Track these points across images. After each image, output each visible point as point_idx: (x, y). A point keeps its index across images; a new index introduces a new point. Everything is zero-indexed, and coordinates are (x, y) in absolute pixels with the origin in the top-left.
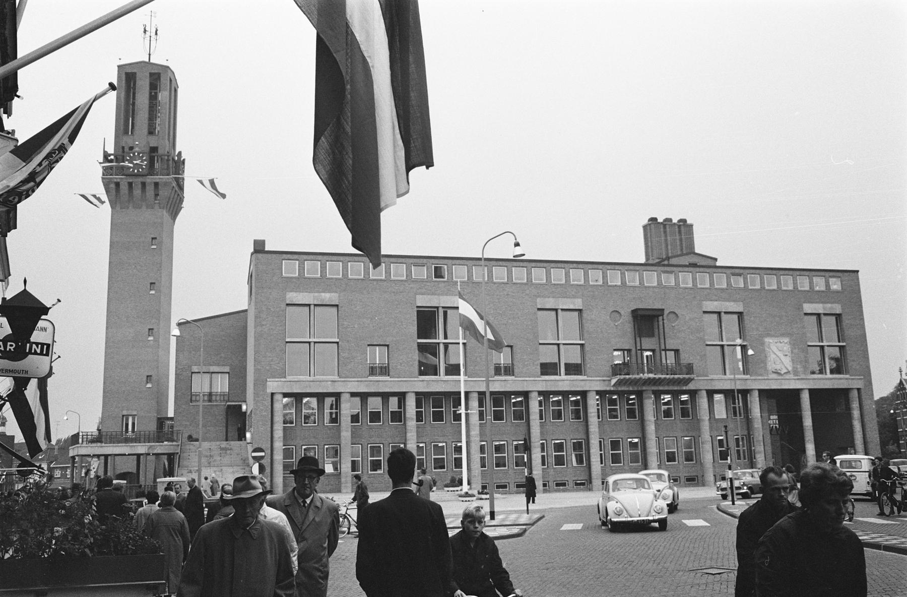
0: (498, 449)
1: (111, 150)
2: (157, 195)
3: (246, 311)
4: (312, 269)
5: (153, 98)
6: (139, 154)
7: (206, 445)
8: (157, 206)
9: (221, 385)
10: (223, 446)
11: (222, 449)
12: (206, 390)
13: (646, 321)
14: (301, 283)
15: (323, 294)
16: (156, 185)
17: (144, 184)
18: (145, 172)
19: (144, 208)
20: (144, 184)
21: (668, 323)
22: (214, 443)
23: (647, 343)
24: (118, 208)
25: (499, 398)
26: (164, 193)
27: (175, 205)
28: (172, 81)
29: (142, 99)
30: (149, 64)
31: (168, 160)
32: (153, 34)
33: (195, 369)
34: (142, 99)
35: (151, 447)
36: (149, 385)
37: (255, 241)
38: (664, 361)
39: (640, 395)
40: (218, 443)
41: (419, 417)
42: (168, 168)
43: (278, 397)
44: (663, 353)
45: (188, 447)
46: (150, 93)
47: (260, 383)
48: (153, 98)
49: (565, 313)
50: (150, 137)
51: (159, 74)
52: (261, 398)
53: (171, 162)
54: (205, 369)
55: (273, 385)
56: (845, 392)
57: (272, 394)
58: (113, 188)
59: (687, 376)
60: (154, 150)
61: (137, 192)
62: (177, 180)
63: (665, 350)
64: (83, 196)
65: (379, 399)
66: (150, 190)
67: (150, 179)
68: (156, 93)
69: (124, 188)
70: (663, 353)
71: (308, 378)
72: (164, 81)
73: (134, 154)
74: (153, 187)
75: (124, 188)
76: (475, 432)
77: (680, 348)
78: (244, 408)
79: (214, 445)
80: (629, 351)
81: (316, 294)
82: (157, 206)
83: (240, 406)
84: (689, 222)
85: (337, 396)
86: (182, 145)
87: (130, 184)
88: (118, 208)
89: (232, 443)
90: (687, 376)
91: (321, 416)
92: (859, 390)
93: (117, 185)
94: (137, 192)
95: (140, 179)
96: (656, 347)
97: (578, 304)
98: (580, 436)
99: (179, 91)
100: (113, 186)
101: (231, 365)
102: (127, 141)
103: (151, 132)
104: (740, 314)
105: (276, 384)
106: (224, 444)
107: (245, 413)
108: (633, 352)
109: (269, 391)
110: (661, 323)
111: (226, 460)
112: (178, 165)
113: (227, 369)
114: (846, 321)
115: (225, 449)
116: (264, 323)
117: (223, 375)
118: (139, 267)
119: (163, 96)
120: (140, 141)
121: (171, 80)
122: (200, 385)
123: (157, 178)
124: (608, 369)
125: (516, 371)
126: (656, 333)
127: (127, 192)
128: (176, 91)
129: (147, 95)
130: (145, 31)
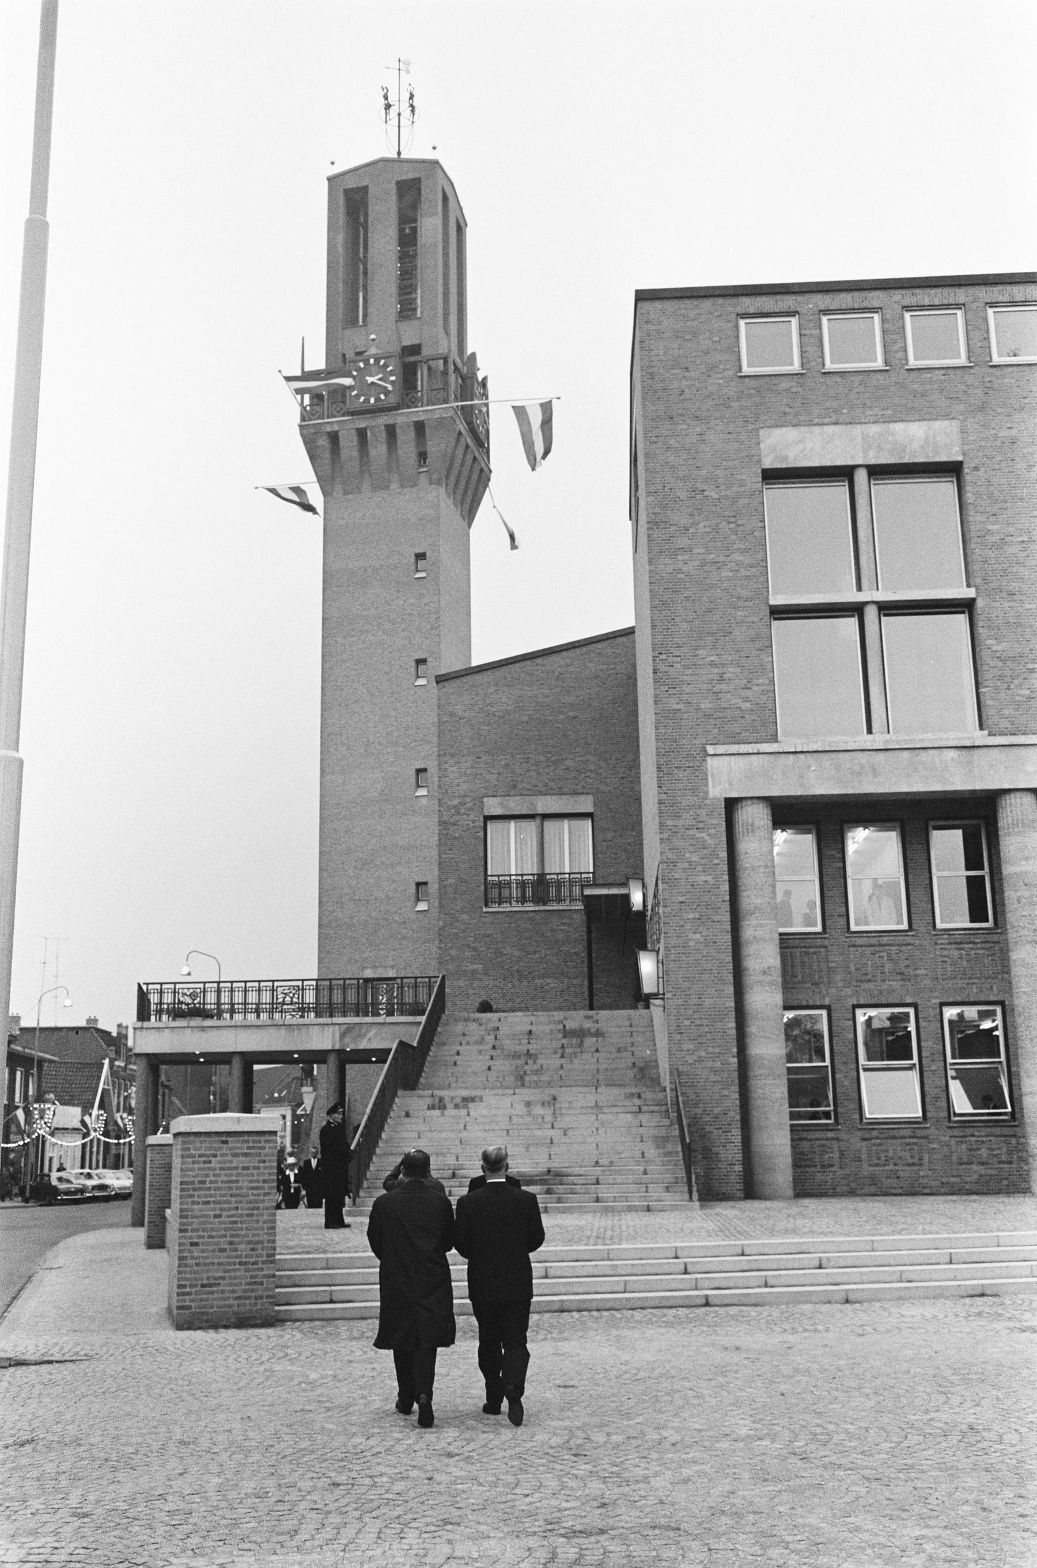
1: (317, 361)
2: (423, 456)
3: (630, 632)
4: (853, 345)
5: (408, 240)
6: (377, 361)
7: (517, 1022)
8: (423, 480)
9: (573, 851)
10: (571, 1025)
11: (566, 1033)
12: (531, 868)
14: (813, 392)
15: (898, 427)
16: (420, 427)
17: (391, 431)
18: (393, 400)
20: (391, 431)
21: (510, 1161)
22: (542, 1016)
26: (437, 445)
27: (470, 483)
28: (448, 199)
29: (383, 243)
30: (399, 161)
31: (445, 373)
32: (406, 112)
33: (493, 806)
34: (383, 243)
35: (350, 1028)
36: (422, 906)
37: (637, 291)
40: (558, 1015)
42: (445, 388)
43: (754, 816)
45: (459, 1028)
46: (401, 231)
47: (684, 763)
48: (408, 240)
50: (404, 326)
51: (417, 181)
52: (687, 819)
53: (452, 377)
54: (515, 805)
55: (728, 773)
57: (731, 805)
58: (323, 447)
60: (415, 349)
61: (378, 450)
62: (468, 413)
64: (273, 491)
66: (407, 442)
67: (405, 417)
68: (414, 230)
71: (866, 741)
72: (430, 196)
73: (366, 362)
74: (412, 434)
78: (637, 898)
79: (544, 1023)
81: (874, 429)
82: (423, 480)
83: (627, 898)
87: (362, 433)
89: (604, 1014)
91: (919, 894)
93: (334, 438)
94: (378, 450)
95: (384, 420)
99: (470, 233)
100: (323, 442)
101: (596, 793)
102: (355, 339)
103: (407, 311)
105: (739, 763)
106: (576, 1019)
107: (642, 914)
109: (718, 790)
111: (585, 1063)
112: (469, 384)
113: (586, 804)
115: (581, 1034)
116: (683, 542)
117: (577, 823)
118: (387, 626)
119: (430, 226)
120: (381, 333)
121: (445, 198)
122: (512, 854)
123: (419, 412)
127: (355, 453)
128: (460, 229)
129: (393, 232)
130: (388, 107)
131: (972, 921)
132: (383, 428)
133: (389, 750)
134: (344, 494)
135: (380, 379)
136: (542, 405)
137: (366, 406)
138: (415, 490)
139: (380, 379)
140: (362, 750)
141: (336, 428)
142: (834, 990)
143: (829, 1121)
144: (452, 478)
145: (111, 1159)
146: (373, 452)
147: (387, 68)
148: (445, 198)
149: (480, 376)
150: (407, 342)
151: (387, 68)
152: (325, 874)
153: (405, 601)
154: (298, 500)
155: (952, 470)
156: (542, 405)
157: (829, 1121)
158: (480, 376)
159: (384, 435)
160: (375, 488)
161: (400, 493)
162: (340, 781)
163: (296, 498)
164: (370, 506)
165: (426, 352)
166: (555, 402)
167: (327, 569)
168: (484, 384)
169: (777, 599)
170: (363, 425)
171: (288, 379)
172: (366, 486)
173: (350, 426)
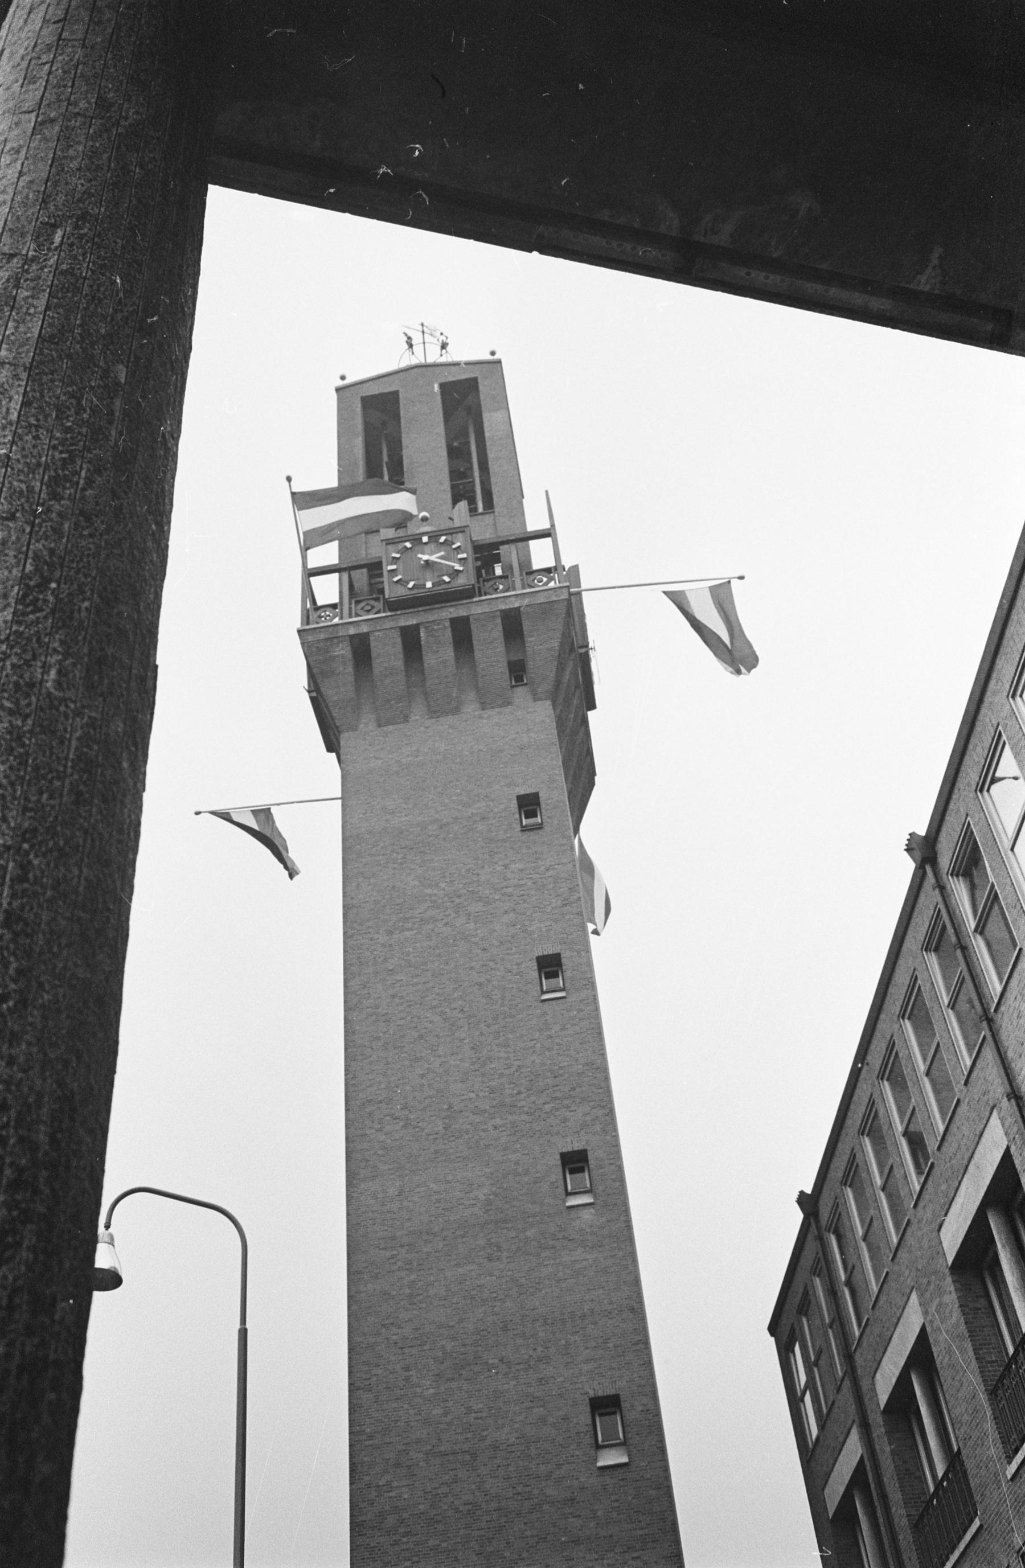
17: (462, 634)
61: (440, 654)
74: (497, 631)
94: (440, 654)
127: (399, 663)
132: (448, 624)
133: (498, 1121)
134: (379, 726)
135: (441, 558)
136: (713, 590)
137: (420, 593)
138: (508, 709)
139: (441, 558)
140: (440, 1127)
141: (364, 629)
145: (425, 442)
146: (430, 660)
147: (197, 813)
151: (197, 813)
152: (366, 1397)
153: (506, 866)
154: (255, 827)
156: (713, 590)
159: (449, 633)
160: (434, 713)
161: (480, 717)
162: (392, 1191)
163: (253, 824)
164: (429, 740)
166: (735, 584)
167: (504, 411)
170: (412, 621)
171: (304, 500)
172: (418, 712)
173: (389, 624)
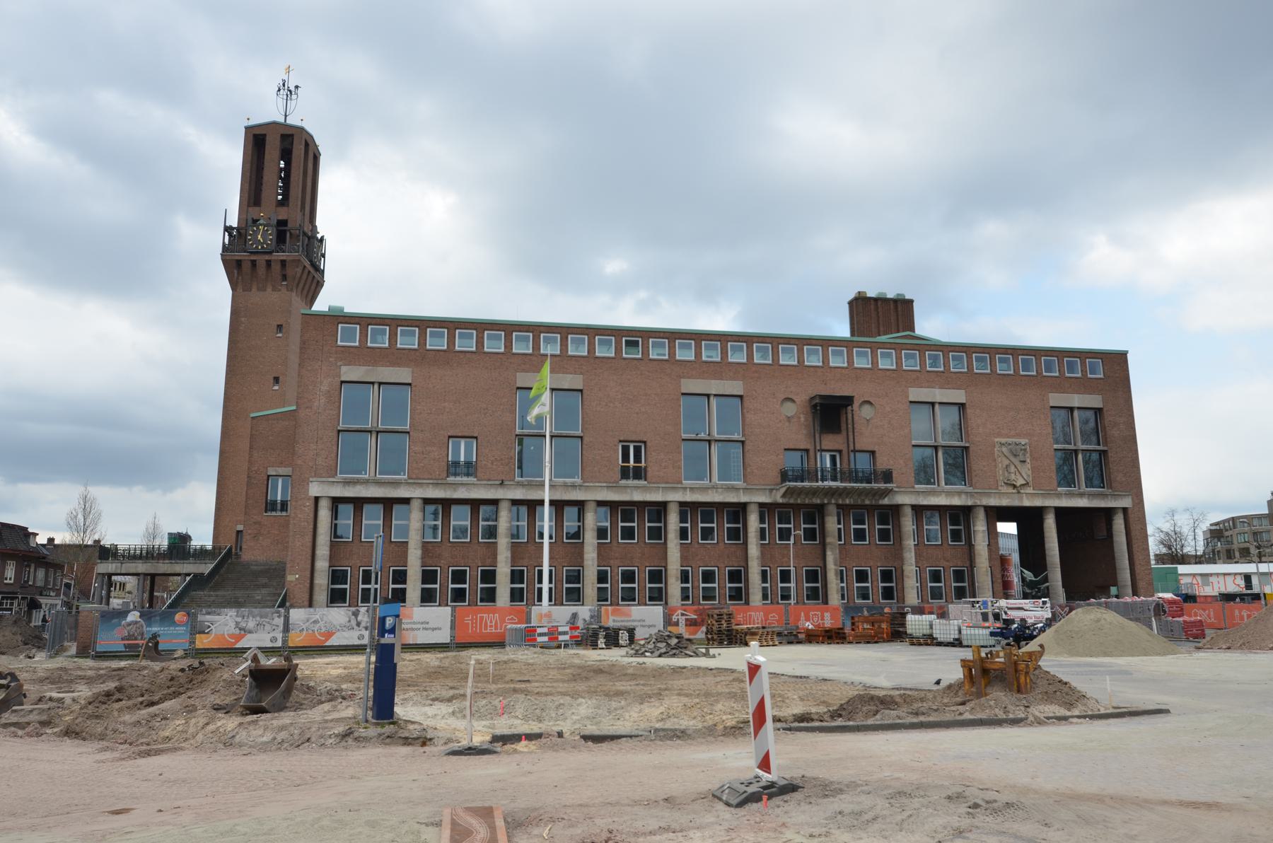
0: (708, 577)
13: (830, 413)
16: (283, 263)
17: (269, 263)
19: (269, 289)
20: (269, 263)
21: (862, 413)
23: (831, 441)
24: (240, 290)
25: (624, 510)
38: (852, 466)
39: (821, 509)
41: (683, 534)
44: (852, 455)
49: (1082, 412)
56: (1109, 513)
57: (317, 499)
59: (882, 486)
60: (282, 223)
63: (855, 451)
65: (467, 508)
66: (276, 268)
69: (246, 267)
70: (852, 455)
75: (246, 267)
76: (300, 544)
77: (876, 449)
80: (807, 451)
84: (871, 293)
85: (580, 505)
86: (323, 225)
88: (240, 290)
90: (882, 486)
92: (1125, 510)
94: (261, 270)
95: (267, 257)
96: (843, 447)
97: (959, 396)
98: (962, 565)
104: (962, 406)
108: (812, 453)
110: (850, 416)
114: (1108, 418)
121: (307, 145)
124: (774, 475)
125: (649, 475)
126: (843, 426)
131: (1156, 555)
142: (244, 733)
143: (1153, 562)
144: (301, 285)
148: (307, 145)
149: (319, 236)
150: (280, 218)
155: (581, 391)
157: (1153, 562)
158: (319, 236)
160: (258, 289)
165: (290, 225)
168: (322, 240)
169: (519, 385)
